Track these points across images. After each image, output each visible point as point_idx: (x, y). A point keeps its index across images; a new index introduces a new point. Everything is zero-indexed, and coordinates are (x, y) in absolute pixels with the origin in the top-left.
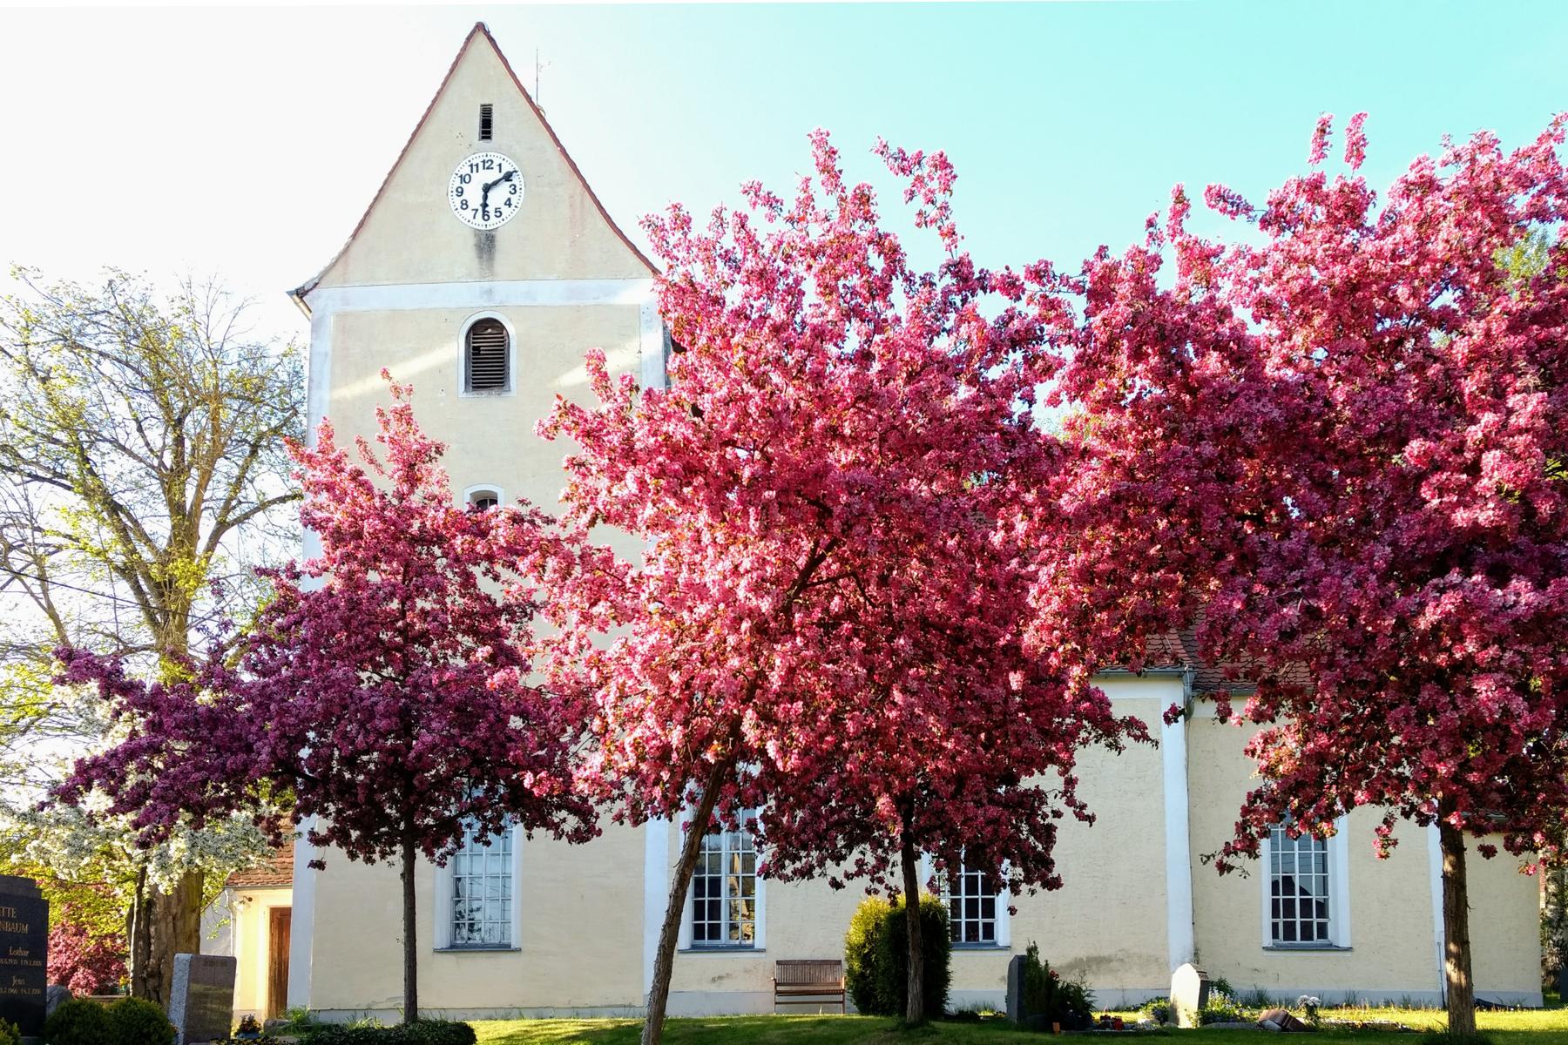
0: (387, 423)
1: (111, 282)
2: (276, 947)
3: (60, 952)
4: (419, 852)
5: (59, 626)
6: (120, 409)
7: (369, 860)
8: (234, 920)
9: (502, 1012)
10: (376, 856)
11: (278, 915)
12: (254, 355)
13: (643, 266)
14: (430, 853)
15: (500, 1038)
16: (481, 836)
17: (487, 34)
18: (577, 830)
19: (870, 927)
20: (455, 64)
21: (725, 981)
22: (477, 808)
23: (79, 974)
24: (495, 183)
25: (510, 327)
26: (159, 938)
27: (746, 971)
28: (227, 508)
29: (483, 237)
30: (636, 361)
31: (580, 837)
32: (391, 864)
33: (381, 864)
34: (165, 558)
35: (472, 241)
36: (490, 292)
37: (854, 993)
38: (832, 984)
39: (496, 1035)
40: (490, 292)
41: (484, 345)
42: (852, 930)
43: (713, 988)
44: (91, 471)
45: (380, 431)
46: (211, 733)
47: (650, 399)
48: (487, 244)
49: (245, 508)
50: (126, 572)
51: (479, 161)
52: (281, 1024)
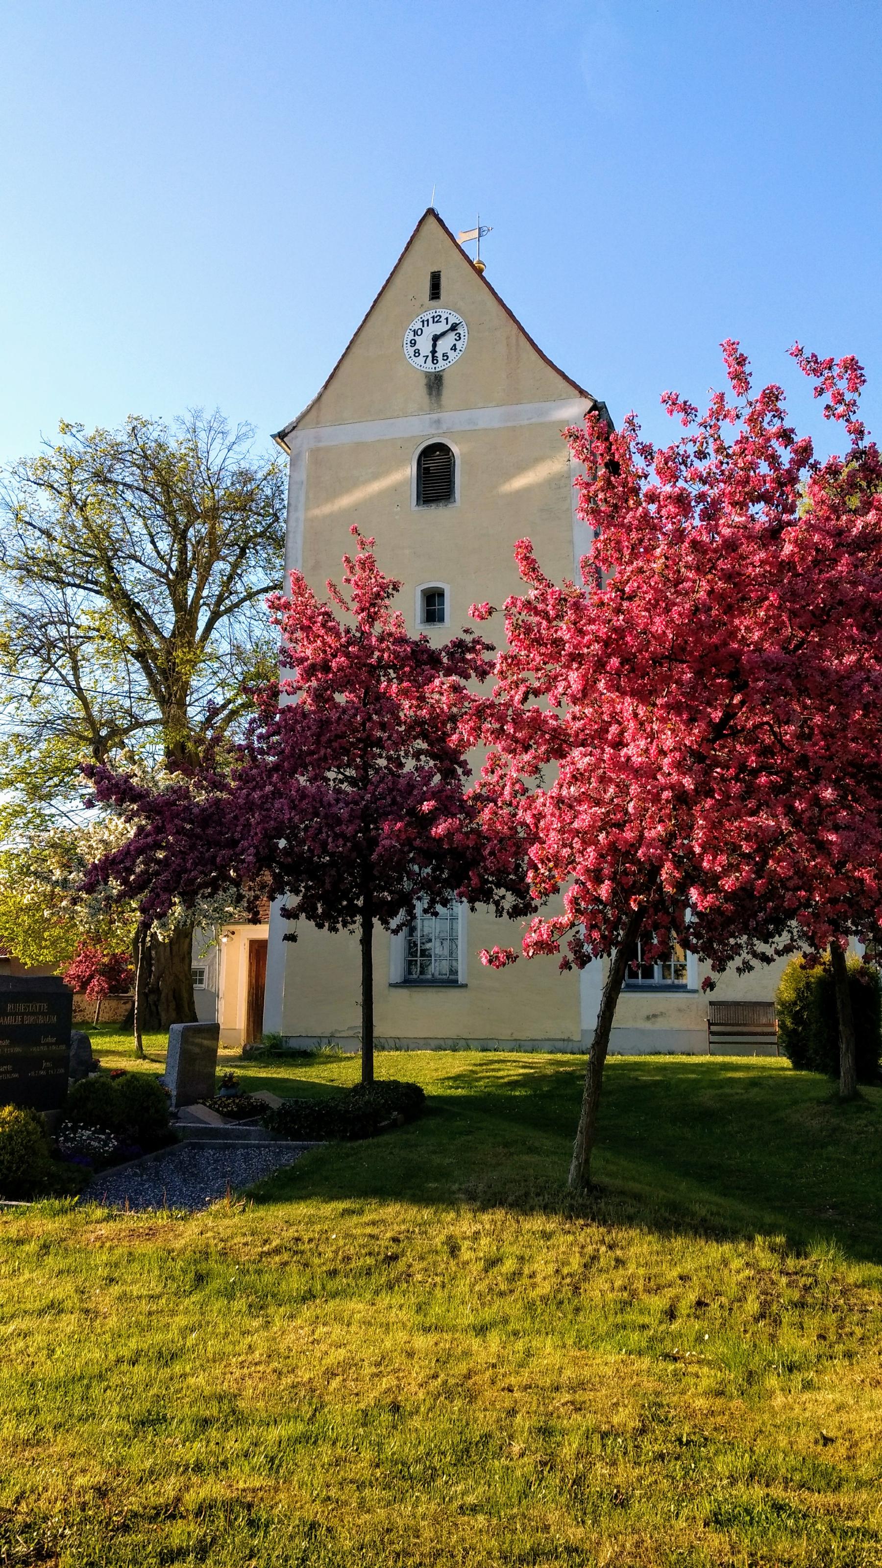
0: (352, 568)
1: (134, 429)
2: (253, 974)
3: (81, 961)
4: (375, 921)
5: (86, 705)
6: (138, 527)
7: (333, 929)
8: (220, 950)
9: (450, 1043)
10: (339, 926)
11: (256, 946)
12: (245, 476)
13: (571, 389)
14: (385, 922)
15: (449, 1078)
16: (430, 907)
17: (437, 216)
18: (515, 907)
19: (801, 985)
20: (410, 243)
21: (659, 1019)
22: (426, 885)
23: (95, 981)
24: (443, 334)
25: (455, 449)
26: (158, 960)
27: (680, 1010)
28: (220, 599)
29: (433, 378)
30: (566, 468)
31: (517, 912)
32: (352, 932)
33: (343, 932)
34: (170, 645)
35: (423, 381)
36: (438, 422)
37: (786, 1047)
38: (765, 1025)
39: (442, 1074)
40: (438, 422)
41: (431, 465)
42: (782, 987)
43: (648, 1026)
44: (115, 578)
45: (347, 574)
46: (203, 830)
47: (577, 609)
48: (435, 383)
49: (234, 599)
50: (140, 656)
51: (429, 317)
52: (257, 1049)
